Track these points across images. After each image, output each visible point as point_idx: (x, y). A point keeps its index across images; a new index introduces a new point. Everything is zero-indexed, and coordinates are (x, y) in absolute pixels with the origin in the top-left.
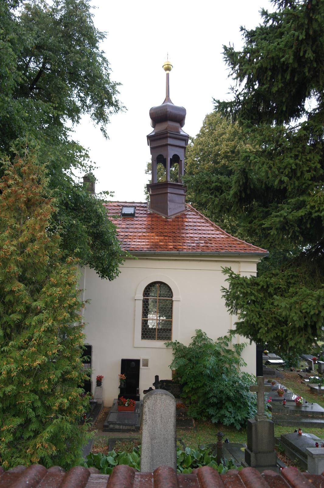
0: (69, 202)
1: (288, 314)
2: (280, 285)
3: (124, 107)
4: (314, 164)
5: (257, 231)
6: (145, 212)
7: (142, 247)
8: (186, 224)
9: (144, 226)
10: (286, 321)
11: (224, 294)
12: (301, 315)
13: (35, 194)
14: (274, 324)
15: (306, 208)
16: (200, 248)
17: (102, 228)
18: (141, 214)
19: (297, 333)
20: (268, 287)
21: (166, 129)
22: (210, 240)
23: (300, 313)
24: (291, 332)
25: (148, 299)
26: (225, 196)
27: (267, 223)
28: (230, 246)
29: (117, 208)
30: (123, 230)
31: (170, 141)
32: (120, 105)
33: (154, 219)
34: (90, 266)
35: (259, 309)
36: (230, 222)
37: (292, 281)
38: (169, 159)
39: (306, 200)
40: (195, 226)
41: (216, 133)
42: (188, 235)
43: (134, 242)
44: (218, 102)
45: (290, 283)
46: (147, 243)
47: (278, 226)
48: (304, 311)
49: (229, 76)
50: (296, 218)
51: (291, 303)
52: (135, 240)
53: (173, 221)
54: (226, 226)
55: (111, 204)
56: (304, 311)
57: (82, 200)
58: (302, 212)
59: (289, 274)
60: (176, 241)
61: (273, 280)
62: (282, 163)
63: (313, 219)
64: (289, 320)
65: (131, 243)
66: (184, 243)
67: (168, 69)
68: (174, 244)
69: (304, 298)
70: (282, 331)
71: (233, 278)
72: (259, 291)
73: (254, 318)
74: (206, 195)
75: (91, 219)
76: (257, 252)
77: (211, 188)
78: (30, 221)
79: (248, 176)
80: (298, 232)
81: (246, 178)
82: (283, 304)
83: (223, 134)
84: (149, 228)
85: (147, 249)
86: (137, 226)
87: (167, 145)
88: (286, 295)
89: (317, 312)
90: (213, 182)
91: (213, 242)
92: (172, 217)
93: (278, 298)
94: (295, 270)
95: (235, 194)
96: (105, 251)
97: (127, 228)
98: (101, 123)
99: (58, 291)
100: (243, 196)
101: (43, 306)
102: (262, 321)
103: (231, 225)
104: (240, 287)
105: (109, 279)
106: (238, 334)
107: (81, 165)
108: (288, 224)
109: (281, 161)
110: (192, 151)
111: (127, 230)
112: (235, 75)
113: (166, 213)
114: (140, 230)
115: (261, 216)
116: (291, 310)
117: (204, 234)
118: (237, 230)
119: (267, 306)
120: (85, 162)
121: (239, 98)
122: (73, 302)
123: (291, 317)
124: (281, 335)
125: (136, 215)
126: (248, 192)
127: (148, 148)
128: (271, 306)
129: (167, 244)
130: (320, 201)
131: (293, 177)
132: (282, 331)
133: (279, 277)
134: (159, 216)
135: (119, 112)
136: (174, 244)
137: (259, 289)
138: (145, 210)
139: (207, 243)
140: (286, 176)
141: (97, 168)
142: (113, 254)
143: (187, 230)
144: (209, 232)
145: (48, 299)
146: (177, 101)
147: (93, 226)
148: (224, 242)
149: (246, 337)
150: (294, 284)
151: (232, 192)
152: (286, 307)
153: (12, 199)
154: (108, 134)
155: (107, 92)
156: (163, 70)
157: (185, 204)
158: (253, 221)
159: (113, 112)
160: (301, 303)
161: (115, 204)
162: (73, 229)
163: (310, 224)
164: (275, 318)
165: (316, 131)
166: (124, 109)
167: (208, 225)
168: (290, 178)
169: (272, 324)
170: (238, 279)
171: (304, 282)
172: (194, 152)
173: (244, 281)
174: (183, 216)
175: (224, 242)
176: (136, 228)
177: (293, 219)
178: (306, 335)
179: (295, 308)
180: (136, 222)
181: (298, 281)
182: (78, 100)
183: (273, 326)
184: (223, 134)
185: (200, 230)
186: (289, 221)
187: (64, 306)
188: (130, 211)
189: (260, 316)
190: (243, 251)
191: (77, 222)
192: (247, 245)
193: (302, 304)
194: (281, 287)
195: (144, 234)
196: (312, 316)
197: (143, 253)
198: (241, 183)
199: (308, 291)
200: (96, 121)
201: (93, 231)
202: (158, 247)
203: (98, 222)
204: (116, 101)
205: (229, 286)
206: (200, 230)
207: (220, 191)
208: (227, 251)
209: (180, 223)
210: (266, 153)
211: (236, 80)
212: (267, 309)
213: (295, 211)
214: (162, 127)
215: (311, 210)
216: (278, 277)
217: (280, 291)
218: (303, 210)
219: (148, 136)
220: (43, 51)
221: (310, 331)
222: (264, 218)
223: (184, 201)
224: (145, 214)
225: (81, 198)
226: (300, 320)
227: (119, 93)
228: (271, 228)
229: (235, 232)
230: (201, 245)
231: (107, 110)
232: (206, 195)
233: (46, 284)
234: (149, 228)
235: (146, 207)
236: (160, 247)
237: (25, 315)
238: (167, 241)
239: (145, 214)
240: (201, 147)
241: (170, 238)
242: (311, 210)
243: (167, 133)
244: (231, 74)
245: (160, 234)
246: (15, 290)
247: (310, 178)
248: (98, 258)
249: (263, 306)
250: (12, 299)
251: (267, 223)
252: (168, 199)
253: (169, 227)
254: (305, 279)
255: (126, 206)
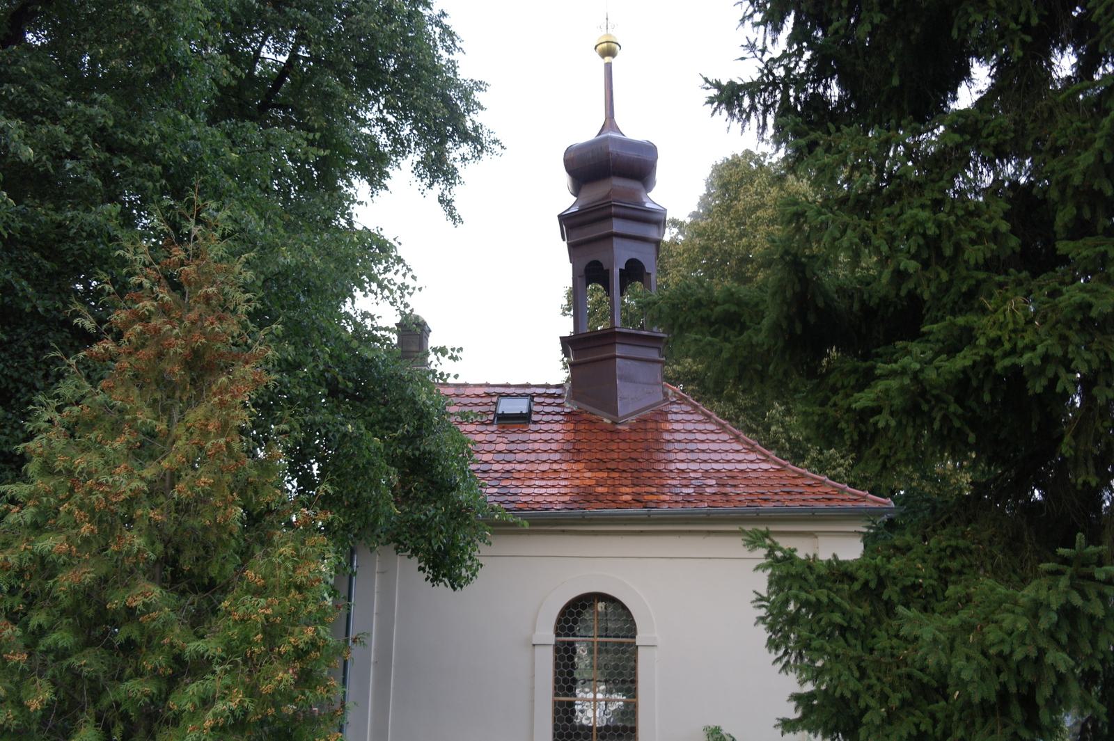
0: (340, 378)
1: (944, 662)
2: (917, 577)
3: (495, 142)
4: (989, 221)
5: (843, 425)
6: (558, 409)
7: (549, 499)
8: (667, 436)
9: (554, 446)
10: (946, 686)
11: (763, 612)
12: (985, 663)
13: (214, 337)
14: (907, 695)
15: (975, 346)
16: (706, 498)
17: (428, 445)
18: (548, 413)
19: (979, 721)
20: (881, 583)
21: (608, 196)
22: (733, 478)
23: (980, 657)
24: (960, 719)
25: (571, 644)
26: (750, 337)
27: (864, 399)
28: (788, 493)
29: (484, 400)
30: (500, 457)
31: (618, 226)
32: (485, 138)
33: (581, 427)
34: (396, 549)
35: (858, 651)
36: (786, 431)
37: (954, 565)
38: (616, 272)
39: (975, 325)
40: (691, 441)
41: (740, 206)
42: (672, 466)
43: (529, 486)
44: (718, 85)
45: (948, 571)
46: (563, 490)
47: (898, 402)
48: (992, 651)
49: (743, 21)
50: (948, 377)
51: (953, 628)
52: (532, 482)
53: (633, 430)
54: (777, 442)
55: (468, 391)
56: (992, 651)
57: (379, 373)
58: (965, 357)
59: (944, 544)
60: (640, 482)
61: (896, 564)
62: (899, 224)
63: (998, 377)
64: (950, 681)
65: (519, 490)
66: (663, 486)
67: (608, 51)
68: (634, 490)
69: (993, 612)
70: (933, 716)
71: (777, 560)
72: (854, 597)
73: (843, 678)
74: (698, 337)
75: (399, 420)
76: (863, 504)
77: (713, 319)
78: (196, 415)
79: (808, 274)
80: (959, 417)
81: (804, 281)
82: (927, 634)
83: (758, 208)
84: (568, 451)
85: (564, 506)
86: (536, 446)
87: (611, 236)
88: (939, 607)
89: (1034, 654)
90: (716, 304)
91: (739, 482)
92: (630, 419)
93: (913, 613)
94: (959, 533)
95: (776, 326)
96: (439, 505)
97: (511, 452)
98: (438, 188)
99: (260, 609)
100: (798, 329)
101: (219, 652)
102: (870, 687)
103: (789, 439)
104: (796, 586)
105: (453, 587)
106: (806, 732)
107: (380, 285)
108: (928, 397)
109: (895, 220)
110: (679, 254)
111: (510, 457)
112: (758, 17)
113: (614, 411)
114: (544, 457)
115: (853, 383)
116: (952, 649)
117: (717, 461)
118: (808, 451)
119: (883, 642)
120: (389, 275)
121: (770, 72)
122: (305, 638)
123: (953, 671)
124: (931, 731)
125: (535, 418)
126: (812, 318)
127: (563, 247)
128: (895, 642)
129: (617, 490)
130: (1015, 322)
131: (933, 260)
132: (933, 716)
133: (913, 556)
134: (593, 418)
135: (484, 155)
136: (634, 490)
137: (857, 593)
138: (559, 405)
139: (724, 485)
140: (913, 257)
141: (420, 289)
142: (459, 515)
143: (669, 451)
144: (730, 456)
145: (235, 632)
146: (632, 128)
147: (401, 440)
148: (771, 482)
149: (820, 736)
150: (960, 573)
151: (766, 323)
152: (935, 641)
153: (150, 351)
154: (460, 210)
155: (453, 108)
156: (596, 56)
157: (664, 387)
158: (828, 399)
159: (470, 157)
160: (982, 628)
161: (480, 391)
162: (349, 448)
163: (992, 392)
164: (910, 676)
165: (989, 135)
166: (497, 148)
167: (725, 437)
168: (926, 265)
169: (900, 695)
170: (792, 564)
171: (989, 567)
172: (685, 255)
173: (810, 567)
174: (658, 418)
175: (771, 482)
176: (534, 451)
177: (941, 379)
178: (1005, 726)
179: (965, 643)
180: (533, 436)
181: (971, 566)
182: (381, 131)
183: (904, 702)
184: (758, 208)
185: (703, 451)
186: (928, 388)
187: (279, 652)
188: (520, 406)
189: (863, 674)
190: (822, 505)
191: (359, 428)
192: (834, 486)
193: (985, 630)
194: (920, 585)
195: (555, 466)
196: (1020, 664)
197: (550, 515)
198: (789, 294)
199: (1001, 590)
200: (427, 181)
201: (403, 454)
202: (591, 498)
203: (419, 428)
204: (476, 129)
205: (766, 584)
206: (703, 451)
207: (738, 328)
208: (779, 504)
209: (649, 436)
210: (851, 203)
211: (762, 28)
212: (884, 650)
213: (944, 356)
214: (597, 192)
215: (990, 352)
216: (911, 555)
217: (919, 597)
218: (966, 351)
219: (560, 216)
220: (287, 9)
221: (1017, 713)
222: (860, 387)
223: (659, 379)
224: (558, 413)
225: (376, 366)
226: (983, 679)
227: (481, 108)
228: (877, 411)
229: (802, 458)
230: (708, 490)
231: (456, 152)
232: (698, 337)
233: (233, 588)
234: (568, 451)
235: (559, 396)
236: (598, 498)
237: (172, 683)
238: (617, 482)
239: (558, 413)
240: (702, 243)
241: (624, 475)
242: (990, 352)
243: (611, 206)
244: (748, 14)
245: (597, 464)
246: (134, 604)
247: (981, 261)
248: (418, 527)
249: (870, 642)
250: (135, 635)
251: (864, 399)
252: (618, 372)
253: (622, 446)
254: (993, 557)
255: (508, 396)
